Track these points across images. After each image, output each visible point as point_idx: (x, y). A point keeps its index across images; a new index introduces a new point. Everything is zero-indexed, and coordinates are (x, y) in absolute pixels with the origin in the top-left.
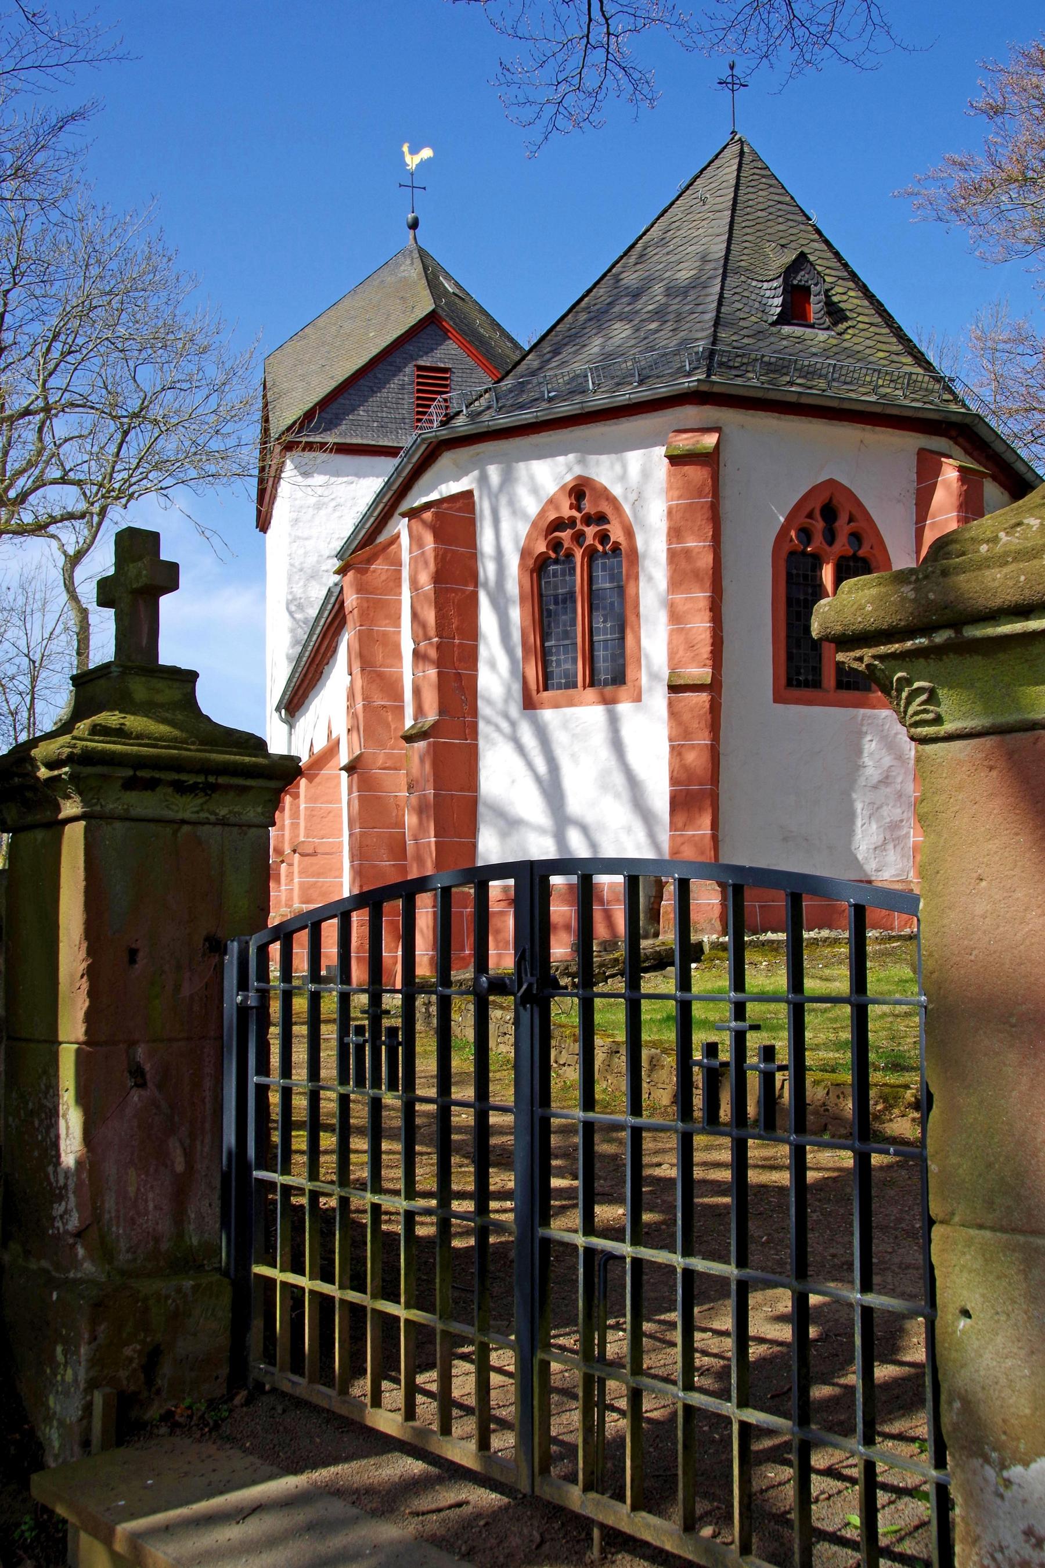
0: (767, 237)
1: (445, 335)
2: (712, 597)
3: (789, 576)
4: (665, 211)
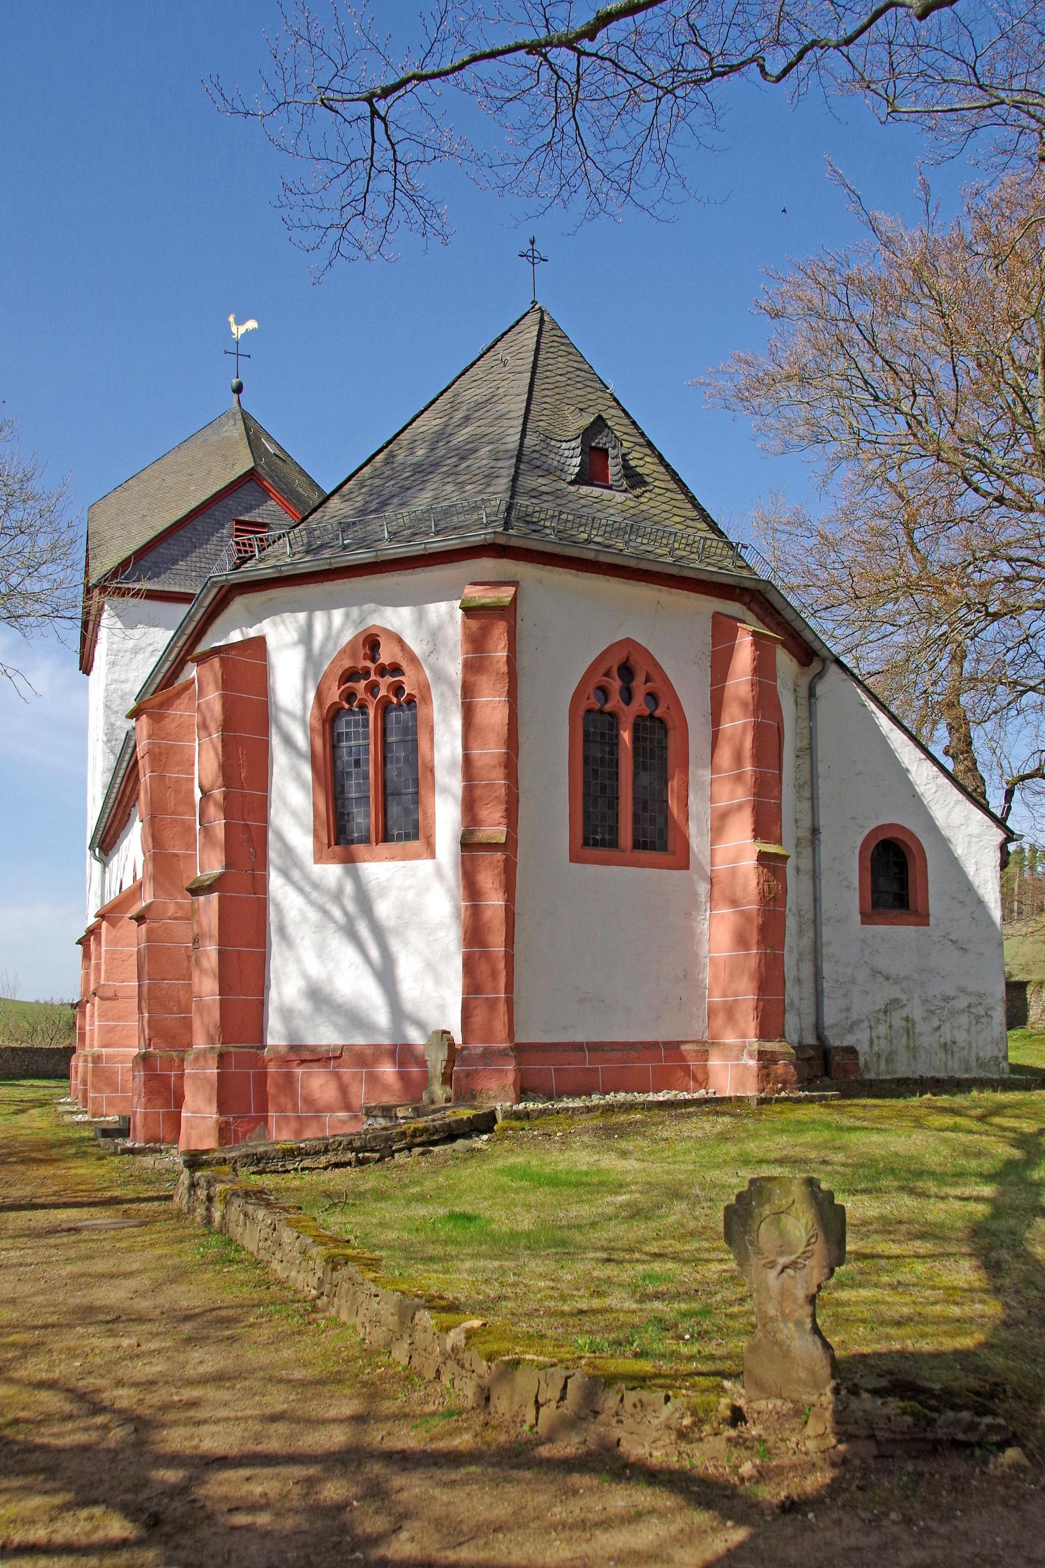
0: (566, 401)
1: (266, 494)
2: (507, 753)
3: (586, 734)
4: (467, 370)
